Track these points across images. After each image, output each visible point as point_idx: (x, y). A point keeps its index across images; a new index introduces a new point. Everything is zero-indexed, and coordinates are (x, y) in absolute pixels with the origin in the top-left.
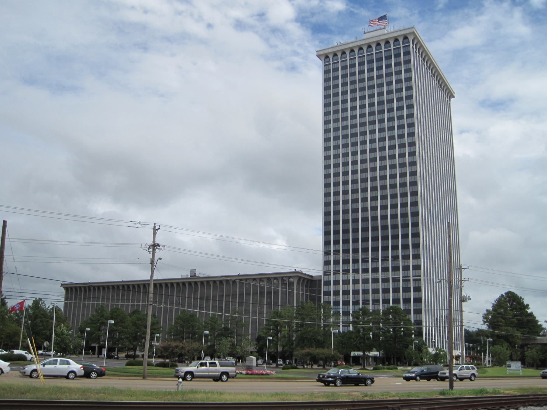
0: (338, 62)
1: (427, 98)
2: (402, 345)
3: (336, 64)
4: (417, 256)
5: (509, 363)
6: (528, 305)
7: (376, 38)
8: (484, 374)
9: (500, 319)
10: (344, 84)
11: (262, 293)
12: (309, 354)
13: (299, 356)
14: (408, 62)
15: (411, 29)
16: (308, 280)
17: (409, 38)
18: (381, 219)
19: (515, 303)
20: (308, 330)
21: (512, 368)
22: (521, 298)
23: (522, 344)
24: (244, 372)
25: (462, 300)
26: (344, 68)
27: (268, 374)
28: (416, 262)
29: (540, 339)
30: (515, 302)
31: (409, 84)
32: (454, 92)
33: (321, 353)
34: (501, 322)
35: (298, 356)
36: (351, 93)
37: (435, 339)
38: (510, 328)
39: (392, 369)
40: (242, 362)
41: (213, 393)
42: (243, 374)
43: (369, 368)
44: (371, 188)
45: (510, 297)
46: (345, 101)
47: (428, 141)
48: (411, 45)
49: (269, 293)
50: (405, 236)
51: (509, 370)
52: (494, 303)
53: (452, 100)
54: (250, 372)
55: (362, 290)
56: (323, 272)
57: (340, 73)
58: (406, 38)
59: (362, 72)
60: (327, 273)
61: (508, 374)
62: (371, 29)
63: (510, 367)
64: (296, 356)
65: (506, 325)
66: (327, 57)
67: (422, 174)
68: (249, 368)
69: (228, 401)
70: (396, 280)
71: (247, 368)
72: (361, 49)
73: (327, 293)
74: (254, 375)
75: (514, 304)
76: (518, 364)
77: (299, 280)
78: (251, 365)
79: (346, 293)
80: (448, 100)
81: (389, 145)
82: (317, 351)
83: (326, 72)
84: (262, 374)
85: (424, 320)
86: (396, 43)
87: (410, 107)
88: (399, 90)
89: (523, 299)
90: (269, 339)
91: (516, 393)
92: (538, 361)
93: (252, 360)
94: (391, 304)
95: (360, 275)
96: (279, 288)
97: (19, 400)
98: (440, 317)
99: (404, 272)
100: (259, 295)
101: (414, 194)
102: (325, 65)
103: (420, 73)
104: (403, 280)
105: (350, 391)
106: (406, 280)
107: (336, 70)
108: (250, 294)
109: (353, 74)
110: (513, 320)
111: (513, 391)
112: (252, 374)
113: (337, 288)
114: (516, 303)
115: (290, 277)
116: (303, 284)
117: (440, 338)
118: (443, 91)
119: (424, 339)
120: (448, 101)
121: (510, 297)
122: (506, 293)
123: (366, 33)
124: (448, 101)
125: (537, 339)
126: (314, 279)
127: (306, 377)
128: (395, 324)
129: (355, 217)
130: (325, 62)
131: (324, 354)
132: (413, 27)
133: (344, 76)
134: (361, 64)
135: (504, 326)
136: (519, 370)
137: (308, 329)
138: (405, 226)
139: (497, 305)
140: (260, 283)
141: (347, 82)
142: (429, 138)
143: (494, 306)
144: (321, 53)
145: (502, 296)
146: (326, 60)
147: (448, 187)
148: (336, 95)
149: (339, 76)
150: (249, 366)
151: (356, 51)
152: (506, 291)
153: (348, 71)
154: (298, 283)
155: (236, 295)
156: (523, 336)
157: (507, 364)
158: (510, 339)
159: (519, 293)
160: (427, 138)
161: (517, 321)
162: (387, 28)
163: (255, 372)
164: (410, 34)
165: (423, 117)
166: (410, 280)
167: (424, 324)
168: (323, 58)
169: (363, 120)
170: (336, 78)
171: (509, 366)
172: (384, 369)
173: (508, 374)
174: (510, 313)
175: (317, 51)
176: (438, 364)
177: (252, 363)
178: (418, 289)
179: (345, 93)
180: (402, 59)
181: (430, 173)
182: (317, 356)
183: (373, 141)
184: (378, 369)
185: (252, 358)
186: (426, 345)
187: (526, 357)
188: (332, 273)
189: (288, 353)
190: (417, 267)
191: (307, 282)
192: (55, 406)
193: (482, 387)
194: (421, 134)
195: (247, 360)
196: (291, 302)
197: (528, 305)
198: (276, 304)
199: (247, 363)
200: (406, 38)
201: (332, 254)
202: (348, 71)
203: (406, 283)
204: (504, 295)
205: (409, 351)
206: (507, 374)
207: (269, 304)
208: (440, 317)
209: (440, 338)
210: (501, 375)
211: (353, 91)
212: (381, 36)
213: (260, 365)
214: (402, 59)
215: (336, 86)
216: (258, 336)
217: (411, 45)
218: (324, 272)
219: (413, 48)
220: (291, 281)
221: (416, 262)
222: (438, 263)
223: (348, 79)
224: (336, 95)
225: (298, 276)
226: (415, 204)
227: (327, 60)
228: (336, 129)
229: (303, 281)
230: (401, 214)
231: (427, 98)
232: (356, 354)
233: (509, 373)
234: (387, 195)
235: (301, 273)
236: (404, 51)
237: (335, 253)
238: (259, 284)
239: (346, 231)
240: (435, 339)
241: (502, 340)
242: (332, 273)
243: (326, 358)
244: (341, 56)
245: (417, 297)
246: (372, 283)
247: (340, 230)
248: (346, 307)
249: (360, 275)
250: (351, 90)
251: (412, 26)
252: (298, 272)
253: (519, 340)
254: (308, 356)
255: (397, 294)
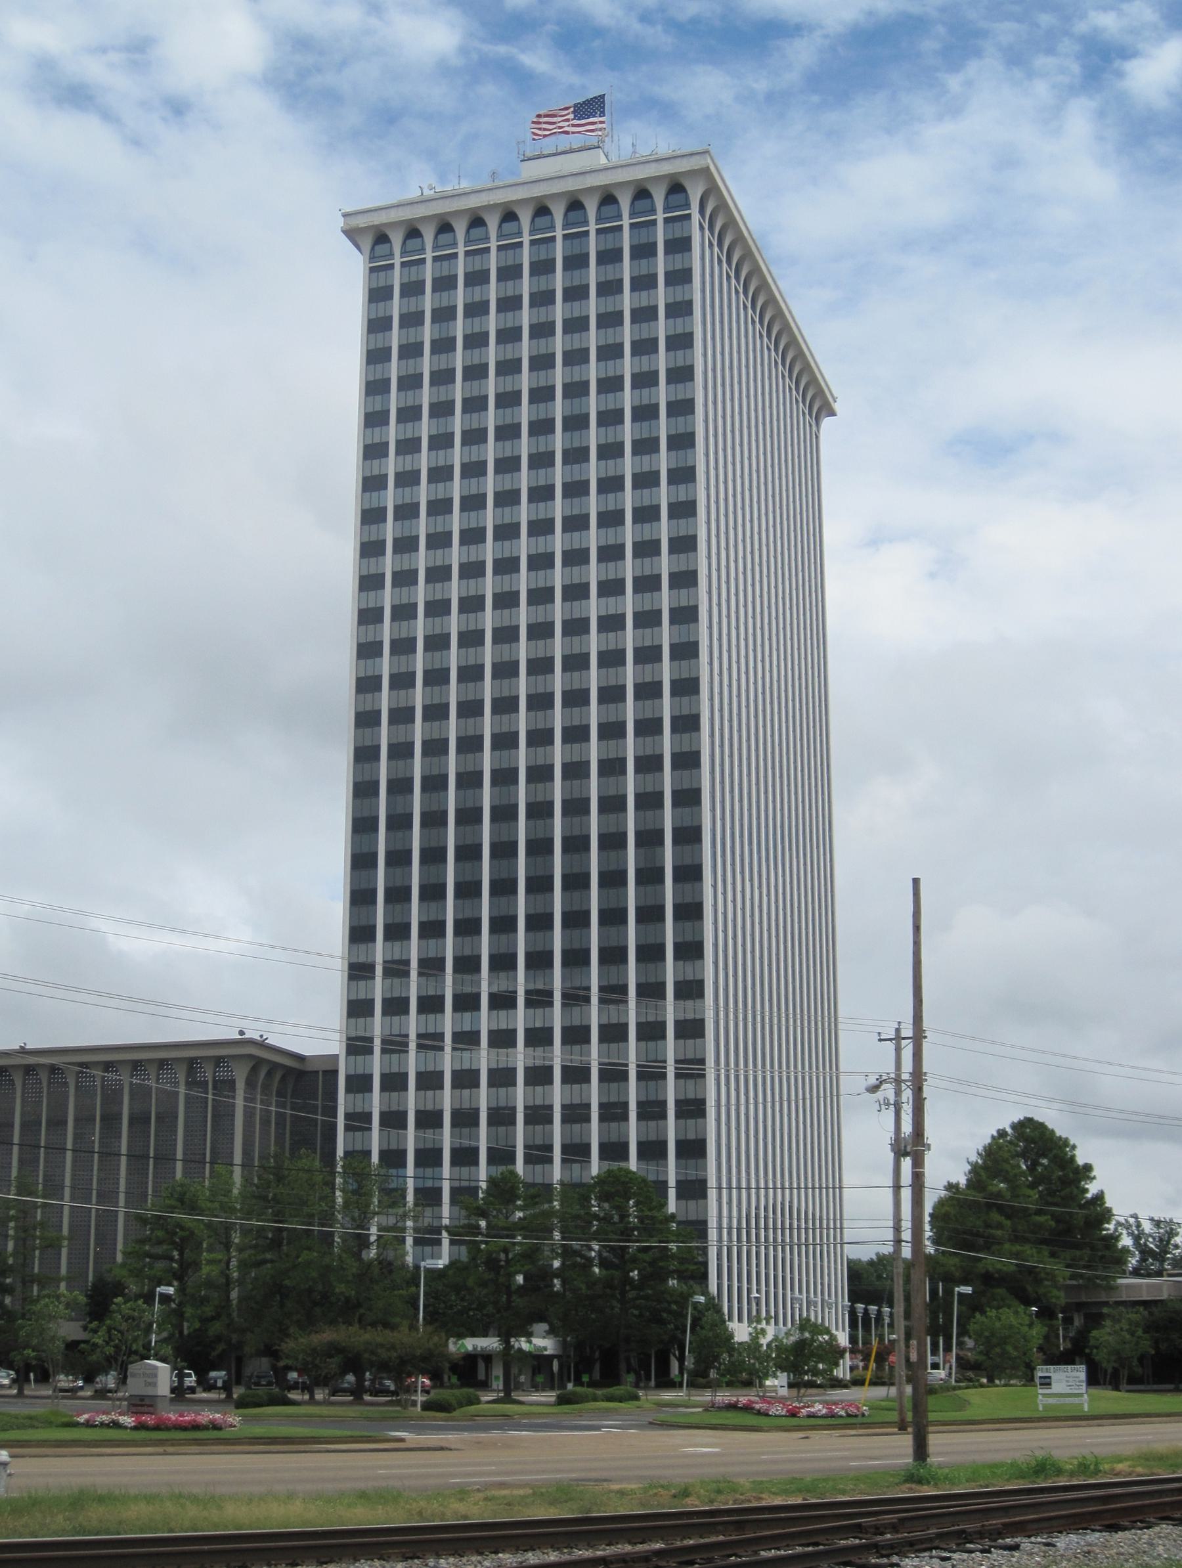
0: (455, 255)
1: (741, 413)
2: (636, 1312)
3: (414, 269)
4: (691, 990)
5: (1047, 1371)
6: (1088, 1168)
7: (570, 180)
8: (960, 1411)
9: (996, 1217)
10: (443, 346)
11: (111, 1121)
12: (334, 1349)
13: (300, 1357)
14: (678, 277)
15: (697, 157)
16: (288, 1071)
17: (689, 191)
18: (493, 855)
19: (1045, 1161)
20: (300, 1259)
21: (1057, 1387)
22: (1066, 1142)
23: (1067, 1303)
24: (128, 1420)
25: (899, 1150)
26: (445, 283)
27: (216, 1427)
28: (689, 1010)
29: (1128, 1286)
30: (1044, 1156)
31: (680, 358)
32: (835, 395)
33: (382, 1346)
34: (1000, 1226)
35: (297, 1359)
36: (465, 378)
37: (758, 1291)
38: (1028, 1249)
39: (621, 1400)
40: (36, 1381)
41: (178, 1498)
42: (126, 1428)
43: (536, 1397)
44: (529, 733)
45: (1028, 1140)
46: (442, 409)
47: (741, 569)
48: (696, 217)
49: (139, 1121)
50: (650, 914)
51: (1044, 1395)
52: (974, 1158)
53: (827, 422)
54: (149, 1419)
55: (418, 1113)
56: (344, 1039)
57: (428, 302)
58: (676, 188)
59: (543, 299)
60: (358, 1046)
61: (1041, 1409)
62: (549, 145)
63: (1049, 1384)
64: (288, 1357)
65: (1016, 1238)
66: (381, 238)
67: (716, 690)
68: (141, 1404)
69: (157, 1530)
70: (613, 1075)
71: (134, 1405)
72: (509, 216)
73: (357, 1122)
74: (168, 1429)
75: (1042, 1165)
76: (1075, 1374)
77: (254, 1070)
78: (149, 1391)
79: (429, 1119)
80: (814, 423)
81: (637, 574)
82: (367, 1336)
83: (378, 295)
84: (196, 1427)
85: (712, 1223)
86: (571, 214)
87: (683, 441)
88: (645, 380)
89: (1074, 1147)
90: (161, 1294)
91: (1139, 1470)
92: (1135, 1363)
93: (156, 1376)
94: (633, 1164)
95: (520, 1057)
96: (213, 1100)
97: (778, 1501)
98: (757, 1208)
99: (643, 1044)
100: (101, 1128)
101: (687, 761)
102: (372, 270)
103: (722, 322)
104: (640, 1076)
105: (590, 1480)
106: (651, 1074)
107: (413, 289)
108: (64, 1123)
109: (476, 309)
110: (1041, 1219)
111: (1128, 1463)
112: (157, 1428)
113: (359, 1103)
114: (1050, 1161)
115: (218, 1061)
116: (266, 1088)
117: (776, 1286)
118: (797, 392)
119: (713, 1288)
120: (811, 426)
121: (1028, 1140)
122: (1014, 1126)
123: (529, 159)
124: (811, 426)
125: (1117, 1287)
126: (310, 1067)
127: (357, 1433)
128: (622, 1233)
129: (650, 827)
130: (372, 258)
131: (393, 1347)
132: (706, 152)
133: (444, 315)
134: (543, 267)
135: (1010, 1240)
136: (1081, 1395)
137: (298, 1257)
138: (650, 876)
139: (985, 1167)
140: (158, 1080)
141: (454, 339)
142: (744, 558)
143: (975, 1169)
144: (362, 222)
145: (1002, 1133)
146: (407, 242)
147: (801, 739)
148: (410, 382)
149: (455, 307)
150: (142, 1398)
151: (493, 223)
152: (1018, 1116)
153: (493, 292)
154: (250, 1083)
155: (12, 1126)
156: (1073, 1277)
157: (1040, 1374)
158: (1029, 1288)
159: (1057, 1122)
160: (736, 561)
161: (1053, 1223)
162: (608, 145)
163: (169, 1419)
164: (692, 173)
165: (726, 482)
166: (663, 1076)
167: (713, 1235)
168: (367, 243)
169: (507, 483)
170: (412, 320)
171: (1046, 1382)
172: (595, 1399)
173: (1041, 1409)
174: (1029, 1197)
175: (345, 215)
176: (1041, 1372)
177: (155, 1385)
178: (693, 1109)
179: (443, 377)
180: (661, 265)
181: (768, 685)
182: (366, 1356)
183: (472, 570)
184: (577, 1403)
185: (156, 1368)
186: (718, 1310)
187: (1095, 1351)
188: (412, 1046)
189: (221, 1347)
190: (691, 1029)
191: (283, 1078)
192: (655, 1528)
193: (1040, 1454)
194: (718, 543)
195: (134, 1375)
196: (222, 1155)
197: (1088, 1168)
198: (165, 1158)
199: (135, 1386)
200: (676, 188)
201: (414, 974)
202: (493, 292)
203: (652, 1084)
204: (1009, 1130)
205: (704, 1332)
206: (1038, 1410)
207: (138, 1158)
208: (757, 1208)
209: (776, 1286)
210: (1019, 1414)
211: (475, 372)
212: (588, 176)
213: (110, 1391)
214: (661, 265)
215: (411, 351)
216: (93, 1284)
217: (696, 217)
218: (348, 1039)
219: (701, 228)
220: (222, 1074)
221: (689, 1010)
222: (763, 1013)
223: (460, 328)
224: (410, 382)
225: (250, 1056)
226: (688, 798)
227: (381, 249)
228: (406, 512)
229: (269, 1074)
230: (601, 837)
231: (741, 413)
232: (470, 1348)
233: (1045, 1406)
234: (516, 770)
235: (262, 1045)
236: (636, 242)
237: (401, 967)
238: (157, 1081)
239: (613, 879)
240: (758, 1291)
241: (1001, 1291)
242: (412, 1046)
243: (403, 1362)
244: (404, 243)
245: (691, 1136)
246: (527, 1083)
247: (551, 877)
248: (465, 1170)
249: (520, 1057)
250: (466, 369)
251: (704, 148)
252: (252, 1042)
253: (1059, 1289)
254: (331, 1356)
255: (693, 1121)
